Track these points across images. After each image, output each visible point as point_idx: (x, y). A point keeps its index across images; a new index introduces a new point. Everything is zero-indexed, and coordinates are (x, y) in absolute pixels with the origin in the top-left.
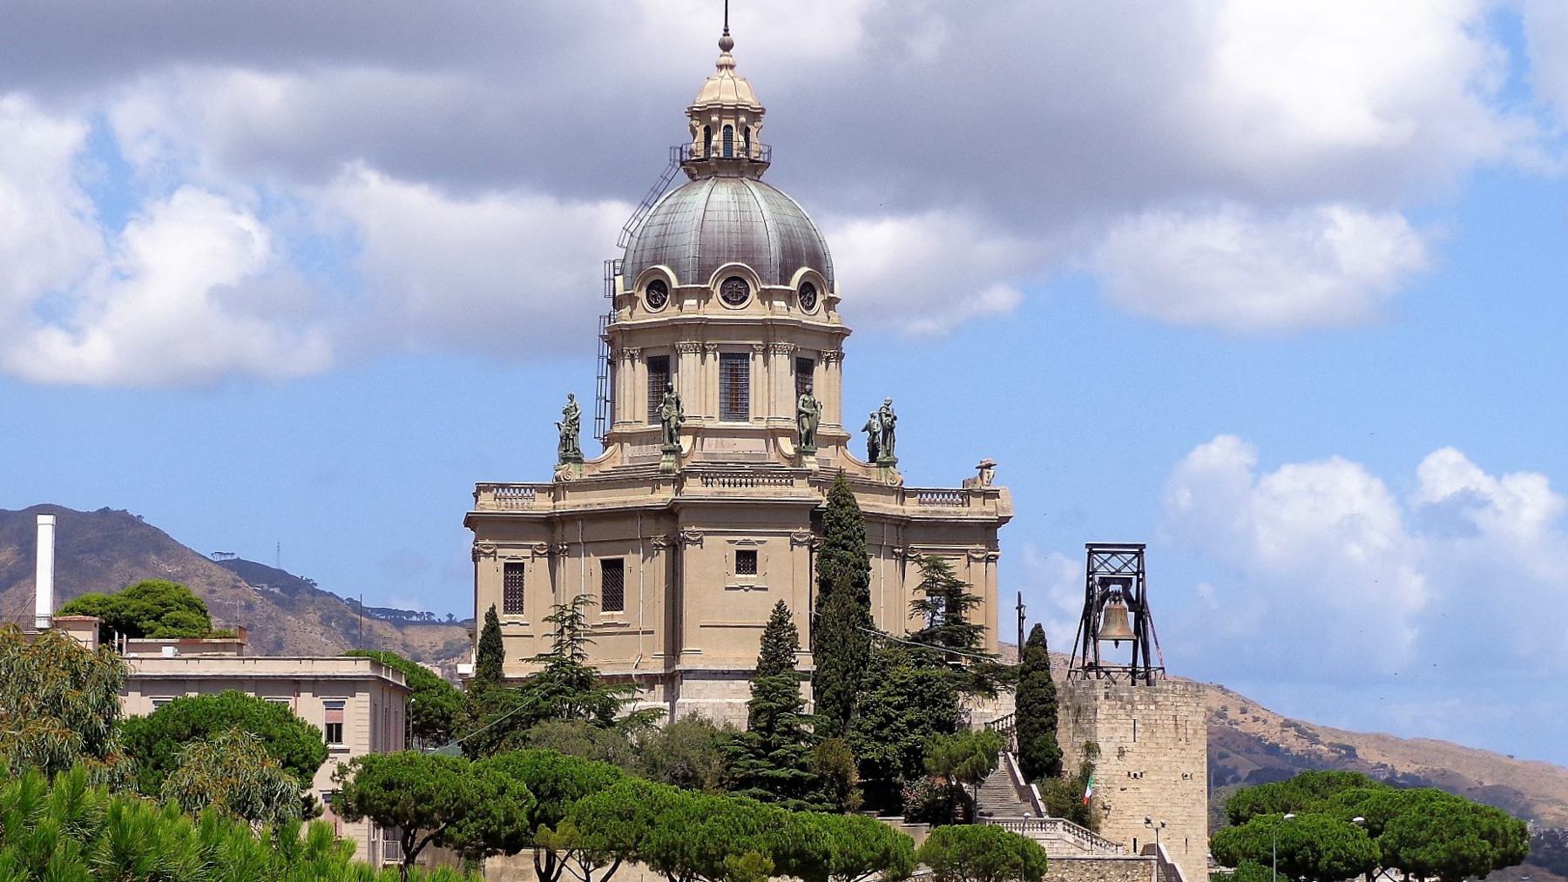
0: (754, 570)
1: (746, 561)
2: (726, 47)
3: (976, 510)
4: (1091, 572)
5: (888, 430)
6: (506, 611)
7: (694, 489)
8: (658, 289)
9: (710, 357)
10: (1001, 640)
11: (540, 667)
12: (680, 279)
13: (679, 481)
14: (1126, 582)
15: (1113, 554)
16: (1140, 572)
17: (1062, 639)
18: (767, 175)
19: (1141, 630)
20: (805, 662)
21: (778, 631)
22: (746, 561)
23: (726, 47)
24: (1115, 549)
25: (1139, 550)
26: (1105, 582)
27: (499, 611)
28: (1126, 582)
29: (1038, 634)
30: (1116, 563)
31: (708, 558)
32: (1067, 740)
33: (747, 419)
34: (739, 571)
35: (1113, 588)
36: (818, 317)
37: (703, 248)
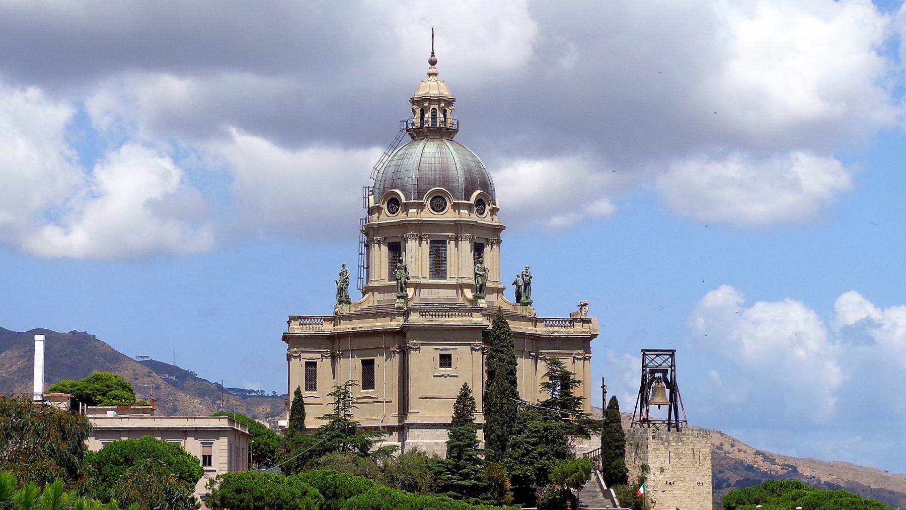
0: (450, 365)
1: (446, 360)
2: (433, 63)
3: (578, 330)
4: (644, 366)
5: (527, 284)
6: (306, 389)
7: (415, 319)
8: (394, 203)
9: (424, 242)
10: (593, 406)
11: (326, 422)
12: (407, 197)
13: (406, 314)
14: (665, 372)
15: (657, 355)
16: (673, 365)
17: (629, 404)
18: (456, 137)
19: (673, 400)
20: (479, 418)
21: (464, 400)
22: (446, 360)
23: (433, 63)
24: (658, 353)
25: (672, 354)
26: (652, 372)
27: (303, 389)
28: (665, 372)
29: (614, 402)
30: (659, 360)
31: (424, 358)
32: (631, 463)
33: (446, 278)
34: (441, 366)
35: (657, 375)
36: (486, 219)
37: (419, 179)
